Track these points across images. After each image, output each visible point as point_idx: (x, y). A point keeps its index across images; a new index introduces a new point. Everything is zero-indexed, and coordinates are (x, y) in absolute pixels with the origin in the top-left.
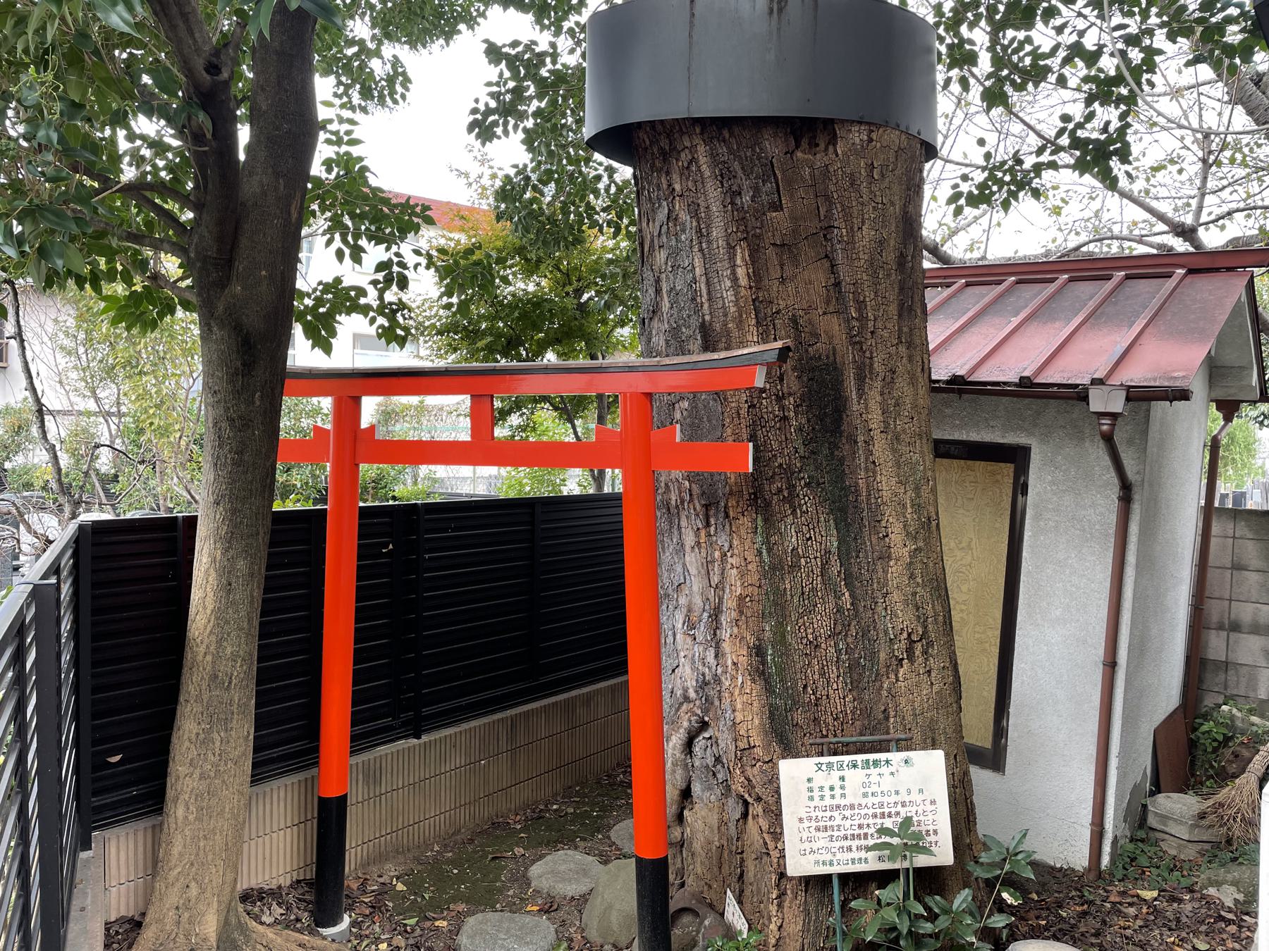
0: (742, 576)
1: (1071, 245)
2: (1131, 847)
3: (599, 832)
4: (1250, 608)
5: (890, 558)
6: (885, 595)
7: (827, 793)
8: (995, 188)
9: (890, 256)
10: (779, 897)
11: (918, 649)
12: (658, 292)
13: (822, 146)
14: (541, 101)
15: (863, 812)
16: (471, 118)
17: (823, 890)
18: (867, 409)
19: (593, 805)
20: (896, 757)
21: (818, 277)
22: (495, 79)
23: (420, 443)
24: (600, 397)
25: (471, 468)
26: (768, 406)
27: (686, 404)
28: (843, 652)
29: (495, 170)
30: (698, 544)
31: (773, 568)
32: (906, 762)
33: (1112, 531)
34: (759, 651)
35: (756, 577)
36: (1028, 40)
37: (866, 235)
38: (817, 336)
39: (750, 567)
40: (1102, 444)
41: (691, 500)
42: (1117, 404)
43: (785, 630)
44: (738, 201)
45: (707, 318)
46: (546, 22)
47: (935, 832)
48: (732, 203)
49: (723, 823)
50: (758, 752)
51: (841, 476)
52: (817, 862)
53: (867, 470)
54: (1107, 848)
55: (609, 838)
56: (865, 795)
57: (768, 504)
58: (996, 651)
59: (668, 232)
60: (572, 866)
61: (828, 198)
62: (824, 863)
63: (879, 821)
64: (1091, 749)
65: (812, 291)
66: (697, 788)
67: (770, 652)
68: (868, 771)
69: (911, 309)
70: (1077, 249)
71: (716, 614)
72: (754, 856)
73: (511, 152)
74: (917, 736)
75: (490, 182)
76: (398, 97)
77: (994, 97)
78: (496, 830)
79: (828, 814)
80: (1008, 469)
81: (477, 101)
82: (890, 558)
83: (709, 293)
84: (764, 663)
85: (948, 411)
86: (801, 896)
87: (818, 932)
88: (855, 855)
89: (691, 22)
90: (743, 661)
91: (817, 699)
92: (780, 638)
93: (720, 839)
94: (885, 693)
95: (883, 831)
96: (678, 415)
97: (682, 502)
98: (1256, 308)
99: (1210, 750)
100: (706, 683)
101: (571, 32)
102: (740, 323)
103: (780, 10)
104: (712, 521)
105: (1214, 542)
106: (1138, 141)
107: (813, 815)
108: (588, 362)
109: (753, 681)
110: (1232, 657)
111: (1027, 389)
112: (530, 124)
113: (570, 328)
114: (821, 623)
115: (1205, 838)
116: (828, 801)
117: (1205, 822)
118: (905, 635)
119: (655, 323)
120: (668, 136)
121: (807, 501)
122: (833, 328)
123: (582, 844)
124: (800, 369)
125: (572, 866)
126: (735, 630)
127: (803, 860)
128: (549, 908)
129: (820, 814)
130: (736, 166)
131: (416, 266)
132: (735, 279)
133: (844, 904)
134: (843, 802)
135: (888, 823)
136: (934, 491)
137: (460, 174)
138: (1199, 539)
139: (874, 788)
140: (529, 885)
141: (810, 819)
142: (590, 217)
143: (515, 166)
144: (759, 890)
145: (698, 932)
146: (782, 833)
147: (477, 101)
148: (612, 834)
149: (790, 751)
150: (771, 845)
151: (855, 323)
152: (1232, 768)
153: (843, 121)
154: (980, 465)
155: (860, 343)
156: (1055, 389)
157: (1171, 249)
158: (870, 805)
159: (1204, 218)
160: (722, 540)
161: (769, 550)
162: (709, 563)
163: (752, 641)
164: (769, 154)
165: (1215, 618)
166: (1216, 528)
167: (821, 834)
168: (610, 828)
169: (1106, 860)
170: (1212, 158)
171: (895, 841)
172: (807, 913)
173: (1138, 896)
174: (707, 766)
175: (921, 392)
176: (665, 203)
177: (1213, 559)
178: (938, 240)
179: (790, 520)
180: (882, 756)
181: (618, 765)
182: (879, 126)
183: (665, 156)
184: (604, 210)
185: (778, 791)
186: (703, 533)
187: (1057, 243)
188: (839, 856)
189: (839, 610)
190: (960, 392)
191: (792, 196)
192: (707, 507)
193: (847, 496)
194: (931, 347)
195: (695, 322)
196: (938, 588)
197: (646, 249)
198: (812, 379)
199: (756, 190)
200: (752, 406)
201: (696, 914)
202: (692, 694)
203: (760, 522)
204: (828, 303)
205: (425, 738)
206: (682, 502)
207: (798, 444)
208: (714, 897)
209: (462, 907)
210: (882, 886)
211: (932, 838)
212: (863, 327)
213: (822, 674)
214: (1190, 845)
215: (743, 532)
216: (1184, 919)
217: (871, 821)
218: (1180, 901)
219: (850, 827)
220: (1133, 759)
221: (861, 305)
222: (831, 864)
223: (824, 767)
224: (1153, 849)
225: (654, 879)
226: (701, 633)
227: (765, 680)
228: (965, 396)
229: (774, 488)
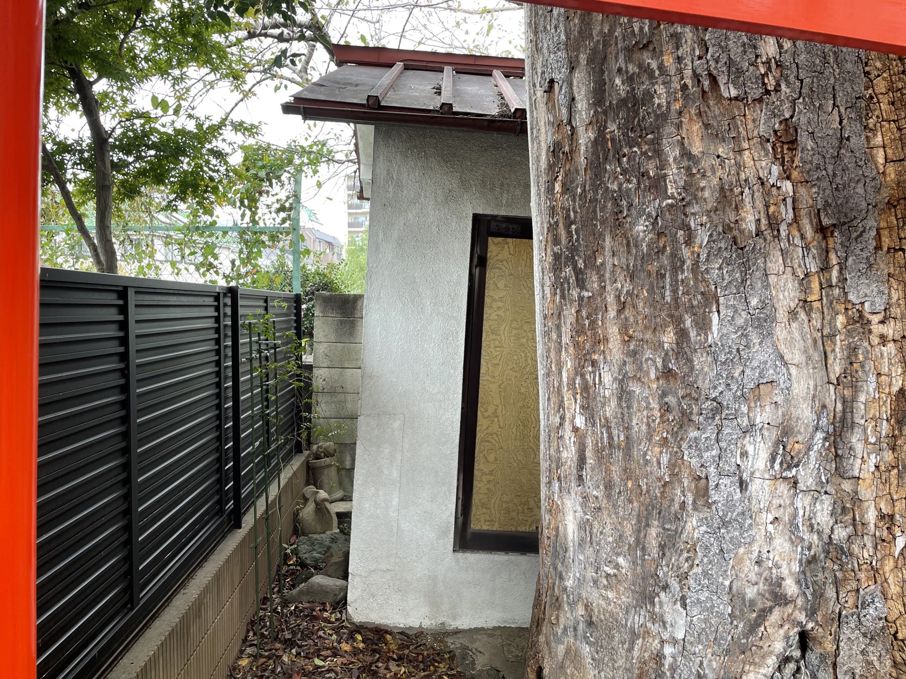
41: (796, 219)
71: (839, 430)
98: (412, 69)
104: (834, 259)
126: (889, 456)
192: (823, 231)
194: (363, 45)
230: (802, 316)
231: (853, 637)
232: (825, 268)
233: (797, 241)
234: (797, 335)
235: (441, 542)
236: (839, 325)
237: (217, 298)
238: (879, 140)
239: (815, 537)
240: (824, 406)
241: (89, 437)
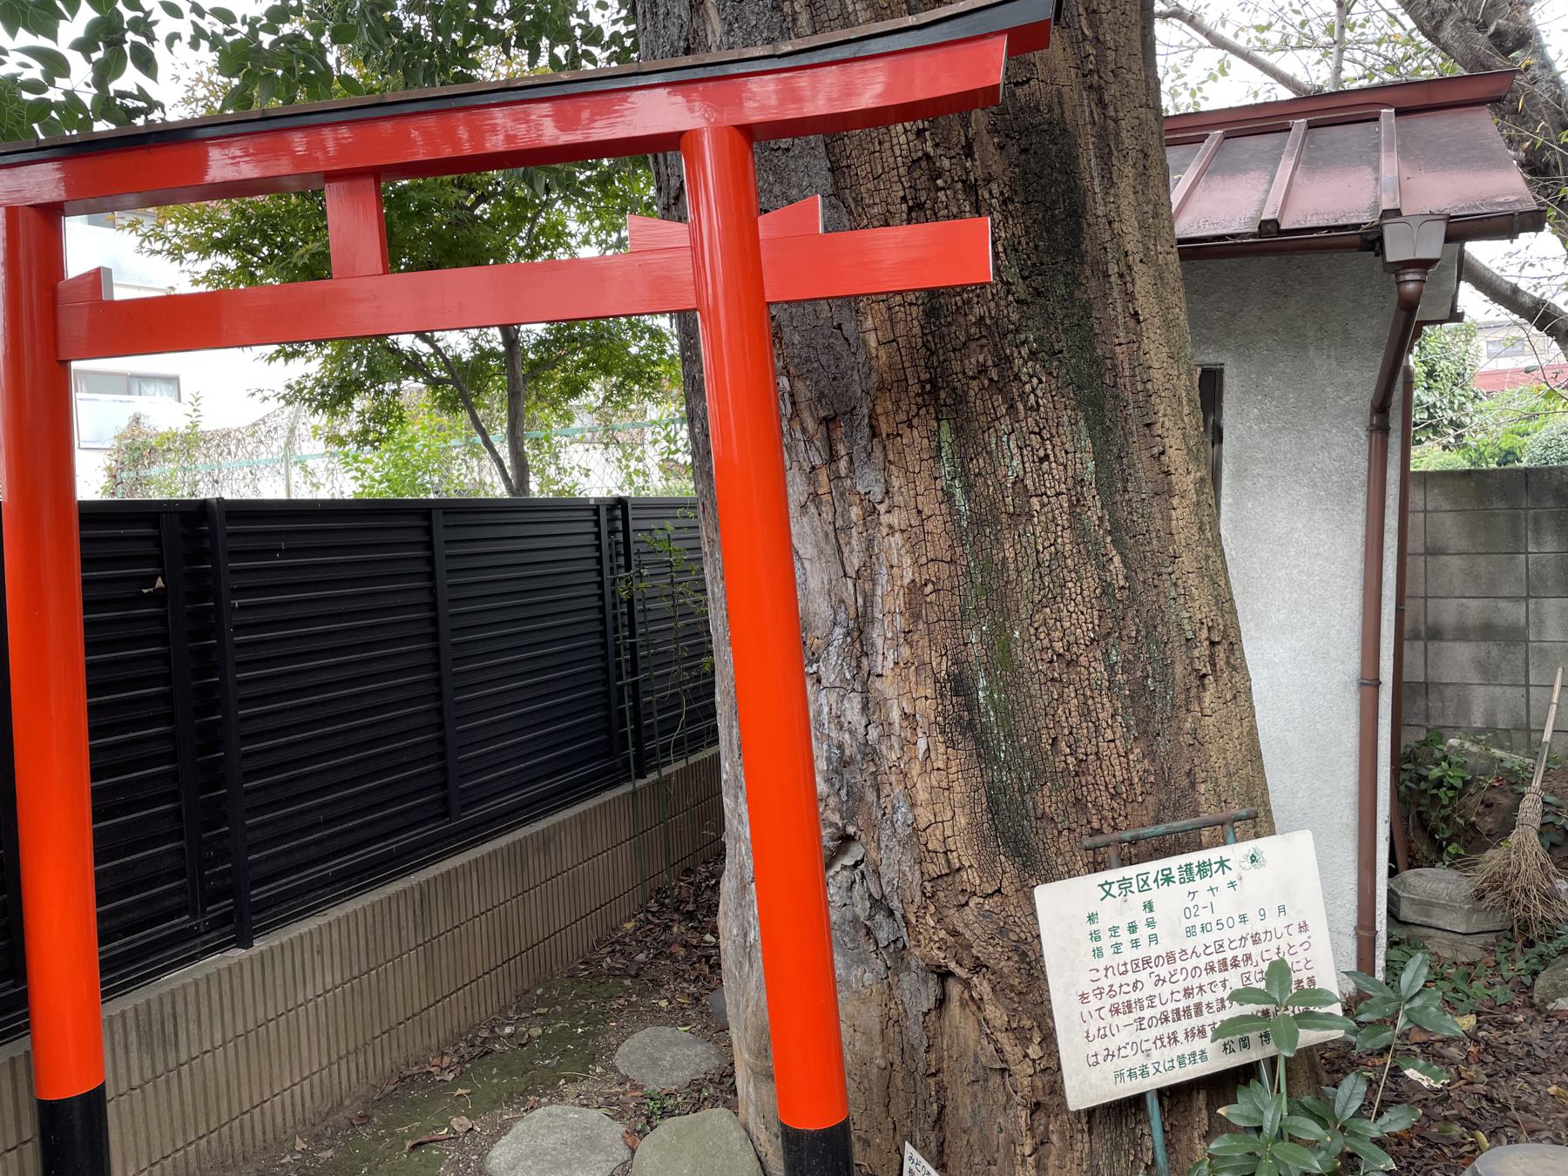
0: (913, 546)
3: (593, 1061)
4: (1453, 604)
7: (1125, 937)
10: (1035, 1150)
15: (1189, 964)
20: (1234, 853)
25: (293, 497)
28: (1118, 668)
30: (815, 497)
31: (978, 521)
32: (1253, 859)
34: (958, 685)
35: (944, 543)
39: (929, 526)
41: (796, 413)
43: (1010, 638)
50: (971, 877)
52: (1119, 1075)
55: (614, 1069)
56: (1190, 932)
57: (960, 398)
60: (567, 1135)
62: (1132, 1074)
67: (982, 683)
68: (1190, 886)
72: (968, 1078)
78: (407, 1090)
79: (1131, 978)
84: (971, 705)
88: (1184, 1048)
90: (926, 709)
93: (886, 1051)
99: (1445, 802)
100: (845, 763)
104: (842, 450)
107: (1105, 983)
109: (951, 744)
110: (1433, 675)
114: (1078, 618)
115: (1486, 927)
116: (1128, 954)
117: (1485, 903)
121: (1037, 385)
123: (571, 1089)
125: (567, 1135)
126: (905, 651)
127: (1095, 1075)
129: (1116, 980)
131: (172, 39)
134: (1154, 950)
139: (1205, 917)
141: (1099, 992)
144: (985, 1142)
148: (618, 1061)
152: (1488, 823)
156: (1323, 233)
158: (1200, 950)
161: (968, 489)
162: (839, 531)
163: (943, 667)
167: (1122, 1019)
168: (611, 1051)
174: (855, 920)
179: (1005, 425)
181: (599, 942)
186: (823, 476)
188: (1156, 1055)
189: (1106, 589)
192: (827, 422)
193: (1101, 376)
198: (1024, 151)
203: (946, 435)
205: (260, 945)
213: (1085, 714)
214: (1467, 939)
219: (1169, 997)
223: (1115, 890)
227: (976, 739)
229: (971, 367)
230: (812, 509)
231: (891, 845)
232: (833, 458)
233: (799, 435)
234: (807, 529)
236: (854, 518)
237: (596, 511)
238: (869, 324)
239: (847, 736)
240: (842, 601)
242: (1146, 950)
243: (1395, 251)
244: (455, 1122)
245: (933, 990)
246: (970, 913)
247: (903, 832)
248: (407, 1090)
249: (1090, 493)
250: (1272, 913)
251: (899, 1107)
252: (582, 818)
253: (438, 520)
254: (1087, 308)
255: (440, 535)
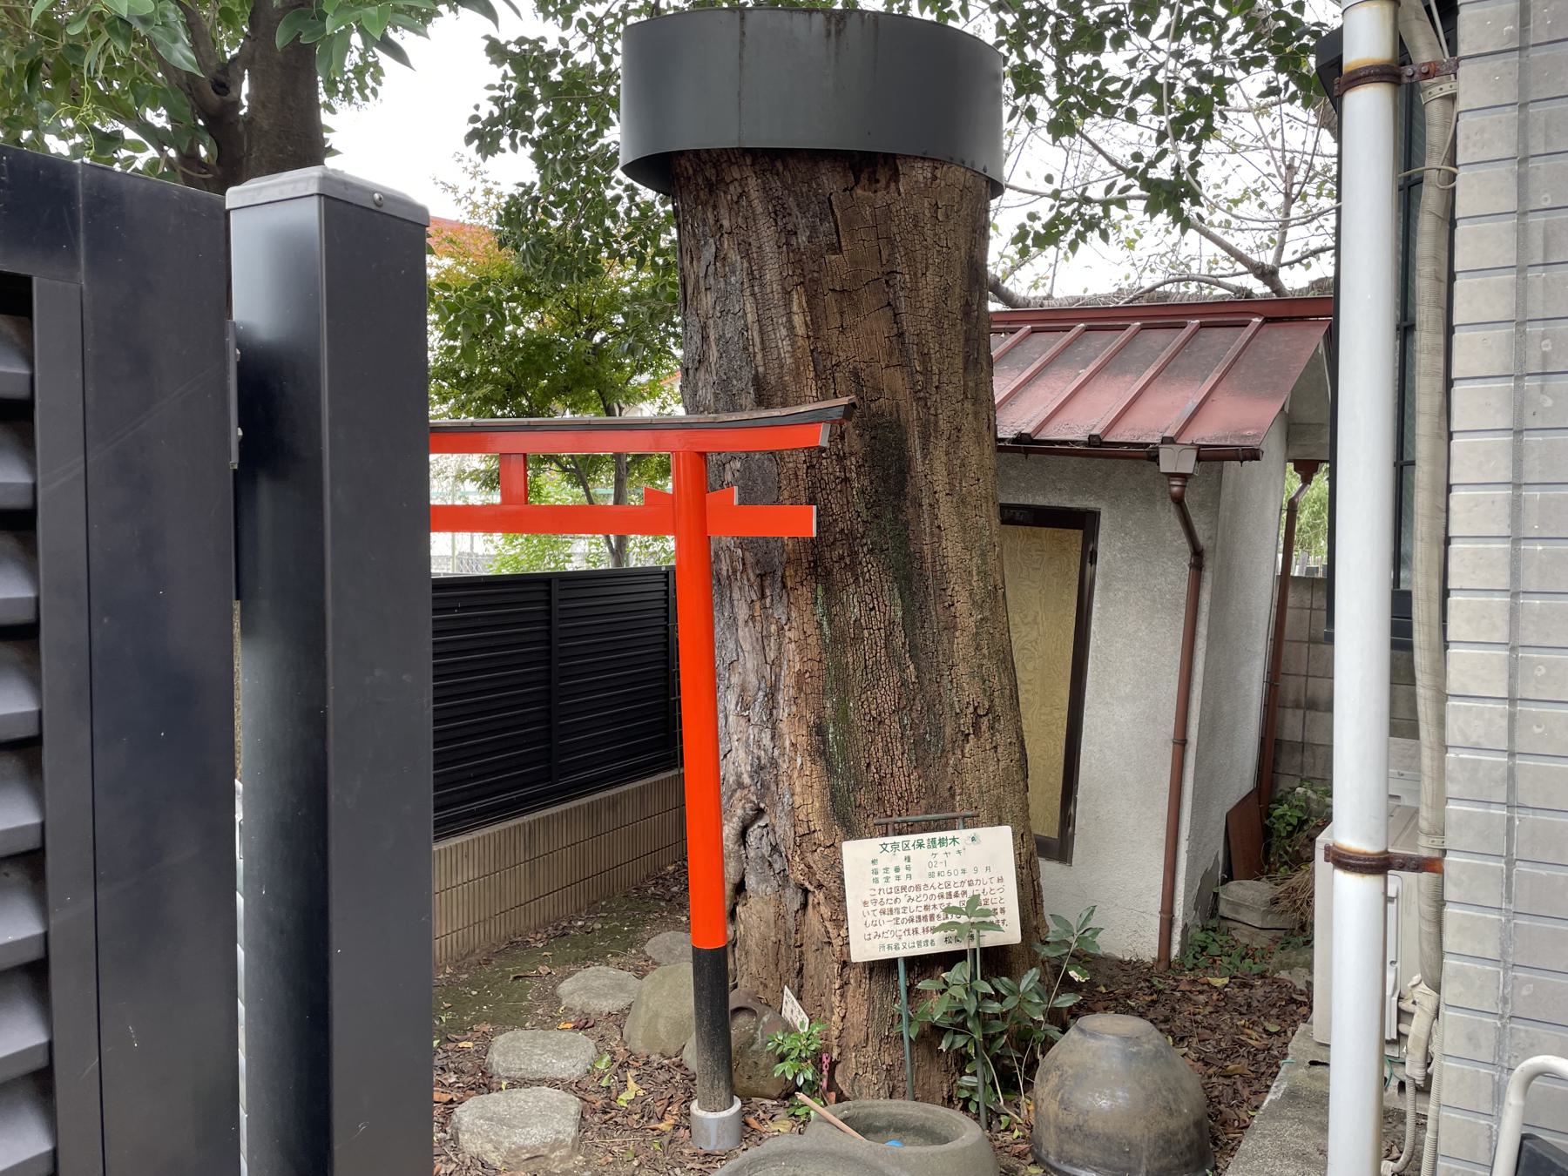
1: (1147, 284)
2: (1202, 936)
5: (955, 628)
6: (951, 668)
7: (892, 874)
8: (1061, 228)
9: (955, 305)
10: (841, 987)
11: (985, 723)
12: (705, 338)
13: (883, 182)
14: (547, 106)
15: (929, 893)
16: (471, 127)
17: (887, 976)
18: (932, 470)
19: (623, 919)
20: (963, 834)
21: (877, 326)
22: (498, 82)
23: (454, 508)
24: (618, 457)
26: (829, 466)
27: (738, 465)
29: (490, 185)
30: (752, 617)
31: (834, 640)
33: (1183, 601)
34: (819, 730)
36: (1096, 65)
37: (930, 283)
38: (880, 391)
40: (1173, 507)
41: (744, 570)
42: (1188, 465)
44: (794, 241)
45: (761, 369)
46: (551, 9)
47: (1003, 910)
48: (788, 244)
49: (780, 916)
50: (819, 836)
51: (906, 541)
53: (932, 534)
54: (1177, 937)
57: (829, 573)
58: (1063, 733)
59: (715, 274)
61: (890, 240)
63: (945, 901)
64: (1160, 833)
65: (874, 342)
66: (751, 882)
69: (977, 361)
70: (1153, 289)
73: (515, 169)
74: (984, 815)
75: (484, 199)
76: (368, 92)
77: (1061, 128)
78: (515, 946)
79: (893, 896)
80: (1076, 535)
81: (477, 107)
82: (955, 628)
83: (762, 341)
84: (825, 742)
85: (1013, 473)
86: (865, 984)
87: (882, 1020)
88: (921, 937)
89: (742, 42)
90: (803, 741)
91: (881, 778)
92: (842, 716)
94: (950, 770)
95: (949, 910)
96: (729, 477)
97: (735, 572)
101: (582, 24)
102: (797, 375)
103: (839, 32)
104: (768, 592)
105: (1290, 613)
106: (1210, 174)
107: (878, 897)
108: (604, 418)
109: (814, 762)
111: (1096, 447)
112: (537, 132)
113: (583, 375)
114: (885, 698)
116: (893, 883)
118: (971, 709)
119: (701, 374)
120: (715, 166)
121: (870, 568)
122: (896, 381)
123: (615, 960)
124: (863, 428)
125: (607, 981)
126: (794, 709)
127: (868, 945)
128: (584, 1025)
130: (791, 202)
132: (791, 327)
133: (909, 989)
134: (908, 883)
135: (955, 902)
136: (1000, 557)
137: (447, 188)
138: (1274, 610)
139: (941, 868)
140: (559, 1003)
142: (608, 244)
143: (521, 185)
144: (820, 983)
145: (756, 1029)
146: (845, 920)
147: (477, 107)
148: (647, 948)
149: (852, 833)
150: (833, 933)
151: (920, 377)
153: (905, 157)
154: (1045, 532)
155: (925, 399)
157: (1249, 294)
159: (1287, 257)
160: (779, 612)
161: (830, 622)
162: (764, 638)
164: (821, 188)
165: (1291, 696)
166: (1292, 600)
167: (886, 917)
168: (644, 942)
169: (1175, 950)
170: (1296, 189)
171: (964, 919)
172: (871, 1000)
173: (1208, 984)
174: (763, 857)
175: (987, 452)
176: (711, 241)
177: (1288, 632)
178: (999, 274)
179: (852, 589)
180: (949, 834)
182: (943, 163)
183: (712, 188)
184: (627, 238)
185: (840, 877)
187: (1131, 281)
190: (1027, 452)
191: (852, 238)
192: (761, 576)
195: (747, 374)
196: (1004, 661)
197: (690, 291)
199: (813, 229)
200: (812, 467)
201: (752, 1012)
202: (746, 780)
203: (820, 592)
204: (890, 355)
206: (735, 572)
207: (861, 507)
208: (770, 997)
209: (487, 1027)
210: (948, 969)
211: (1000, 917)
212: (928, 381)
213: (886, 752)
215: (802, 603)
216: (1255, 1004)
217: (937, 902)
218: (1252, 987)
220: (1203, 844)
221: (925, 357)
222: (897, 947)
224: (1225, 938)
225: (713, 972)
226: (756, 713)
228: (1031, 456)
232: (763, 596)
235: (853, 1011)
241: (319, 443)
242: (903, 882)
243: (1166, 465)
244: (541, 968)
245: (799, 899)
246: (817, 856)
247: (788, 808)
248: (515, 946)
249: (898, 630)
250: (982, 870)
251: (783, 966)
252: (641, 790)
253: (555, 586)
254: (906, 525)
255: (556, 594)
